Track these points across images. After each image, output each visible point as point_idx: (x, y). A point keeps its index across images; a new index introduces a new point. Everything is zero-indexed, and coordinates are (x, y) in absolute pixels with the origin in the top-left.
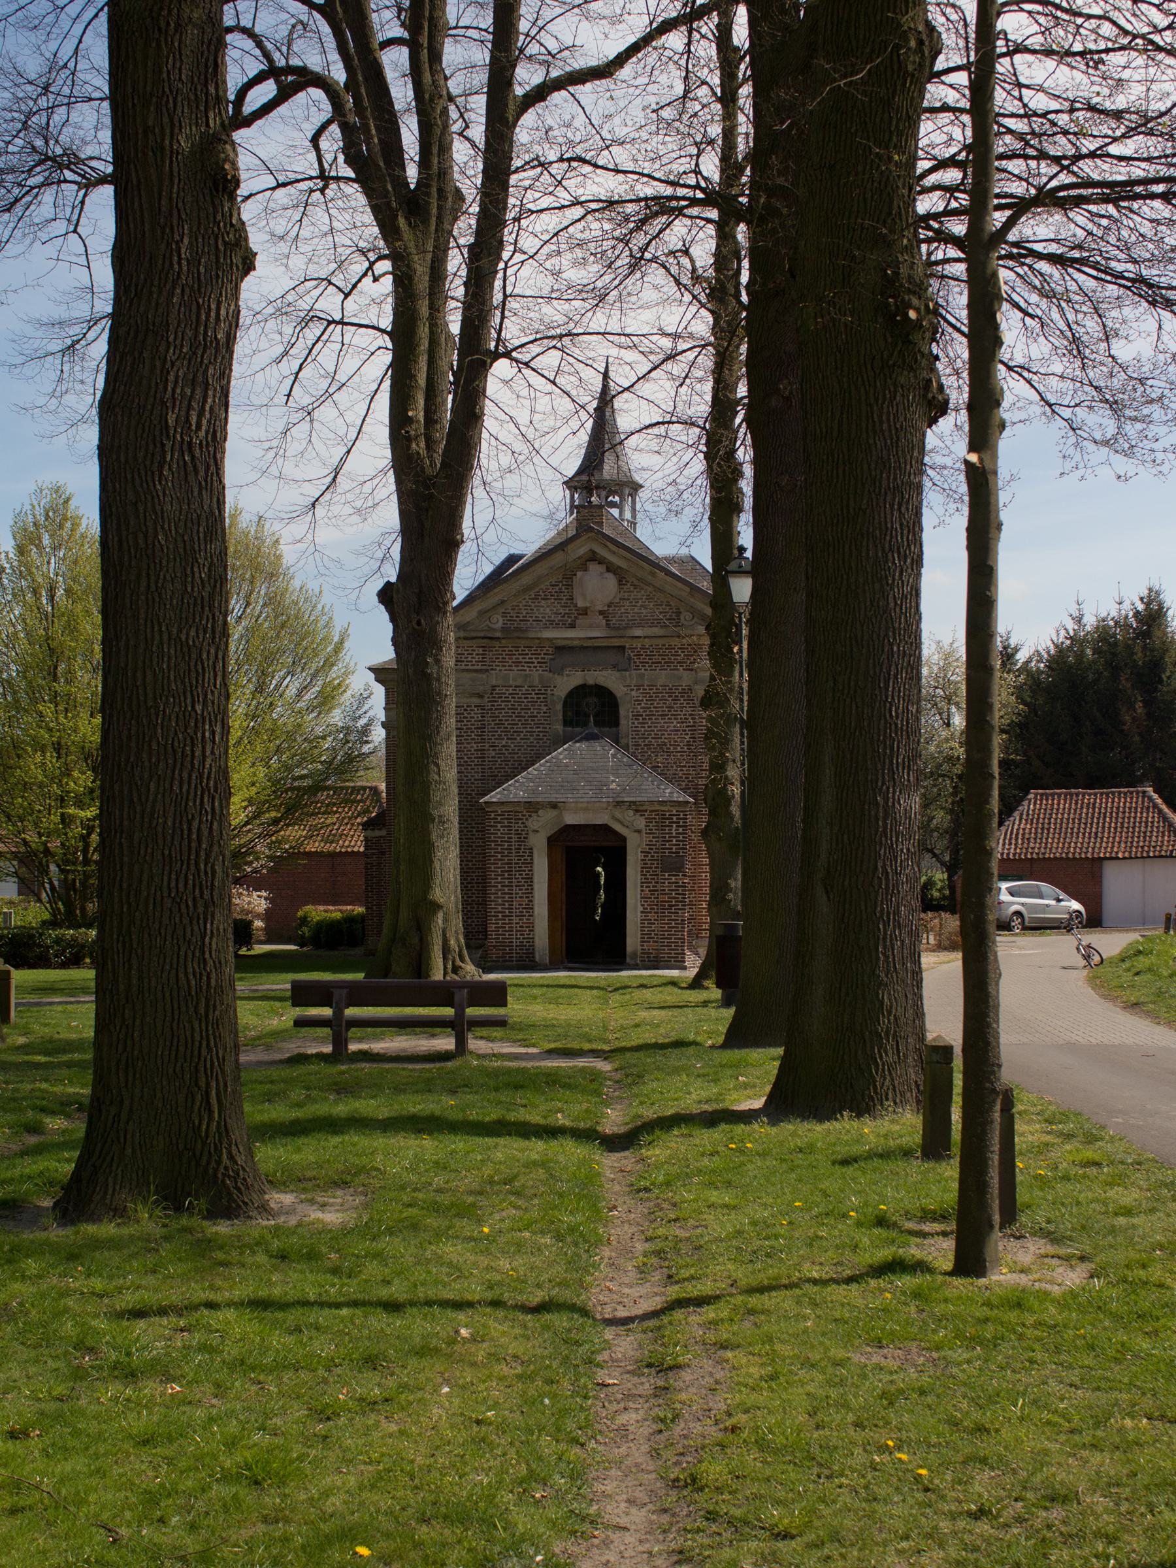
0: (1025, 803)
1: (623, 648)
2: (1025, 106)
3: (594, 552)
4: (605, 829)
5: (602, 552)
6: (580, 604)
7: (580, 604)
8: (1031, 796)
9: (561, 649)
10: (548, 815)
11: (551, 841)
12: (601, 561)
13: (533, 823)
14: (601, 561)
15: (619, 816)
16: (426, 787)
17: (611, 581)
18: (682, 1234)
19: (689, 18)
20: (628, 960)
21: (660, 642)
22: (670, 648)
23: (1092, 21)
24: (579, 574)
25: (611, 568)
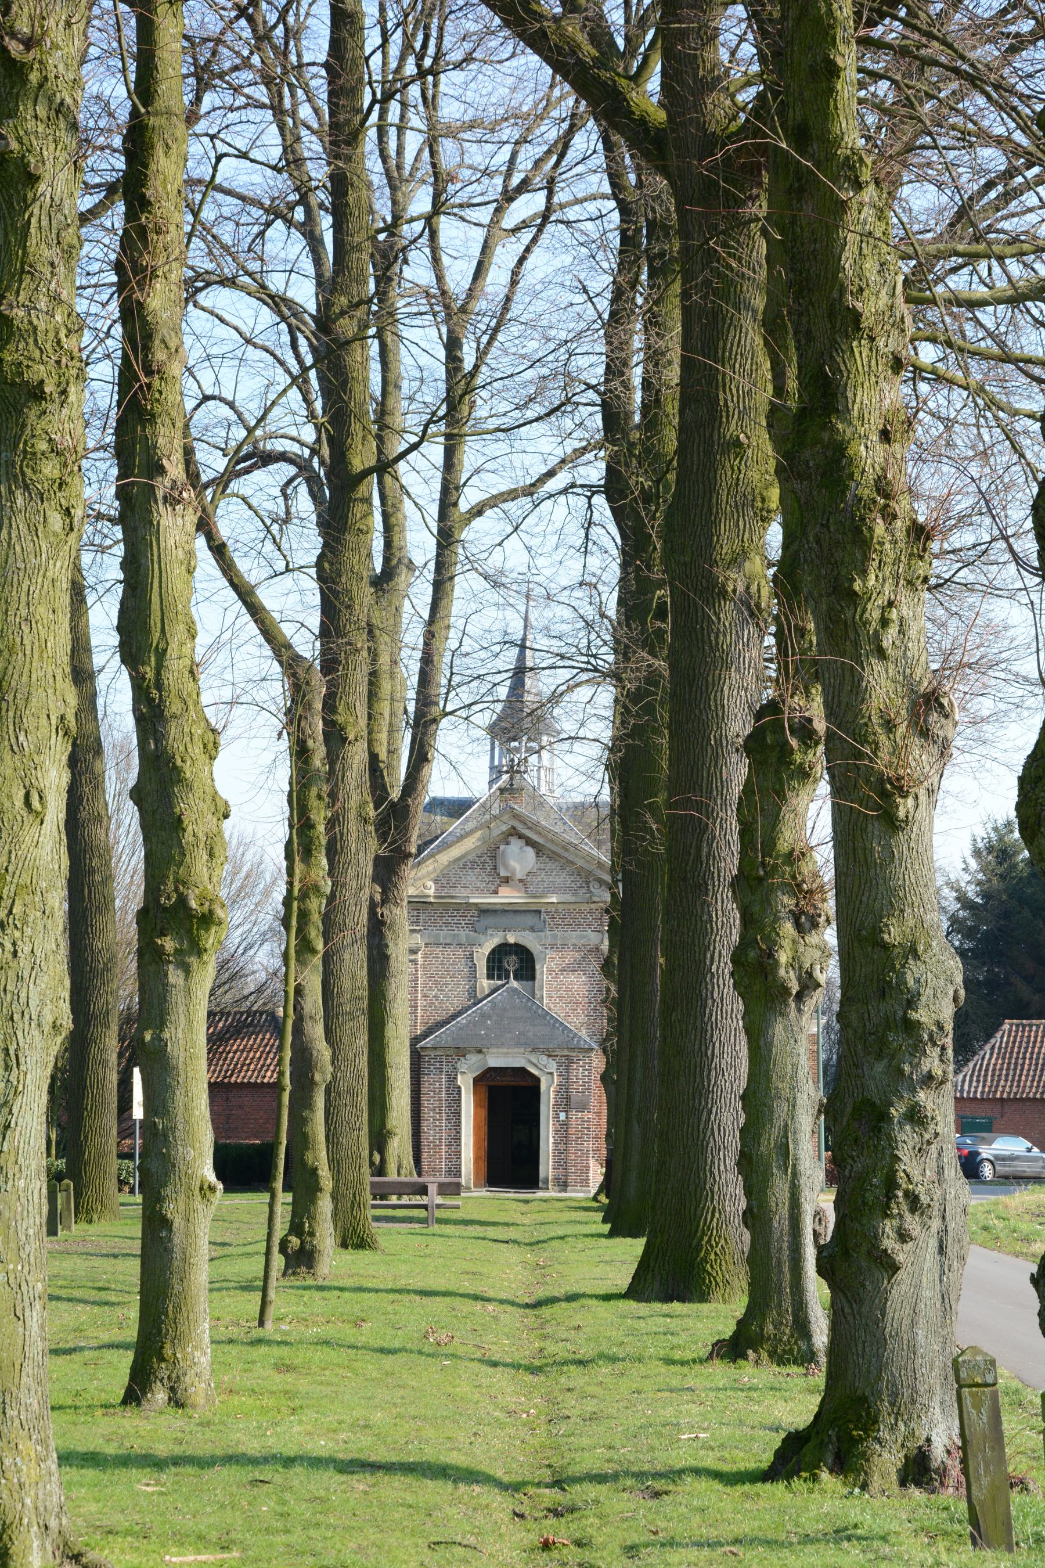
0: (999, 1035)
1: (539, 912)
2: (223, 482)
3: (513, 828)
4: (522, 1071)
5: (520, 827)
6: (503, 873)
7: (503, 873)
8: (1006, 1027)
9: (485, 911)
10: (473, 1059)
11: (477, 1081)
12: (521, 836)
13: (462, 1066)
14: (521, 836)
15: (534, 1061)
16: (383, 1037)
17: (530, 852)
18: (545, 371)
19: (1041, 199)
20: (541, 1184)
21: (572, 907)
22: (580, 912)
23: (492, 427)
24: (502, 847)
25: (529, 842)
